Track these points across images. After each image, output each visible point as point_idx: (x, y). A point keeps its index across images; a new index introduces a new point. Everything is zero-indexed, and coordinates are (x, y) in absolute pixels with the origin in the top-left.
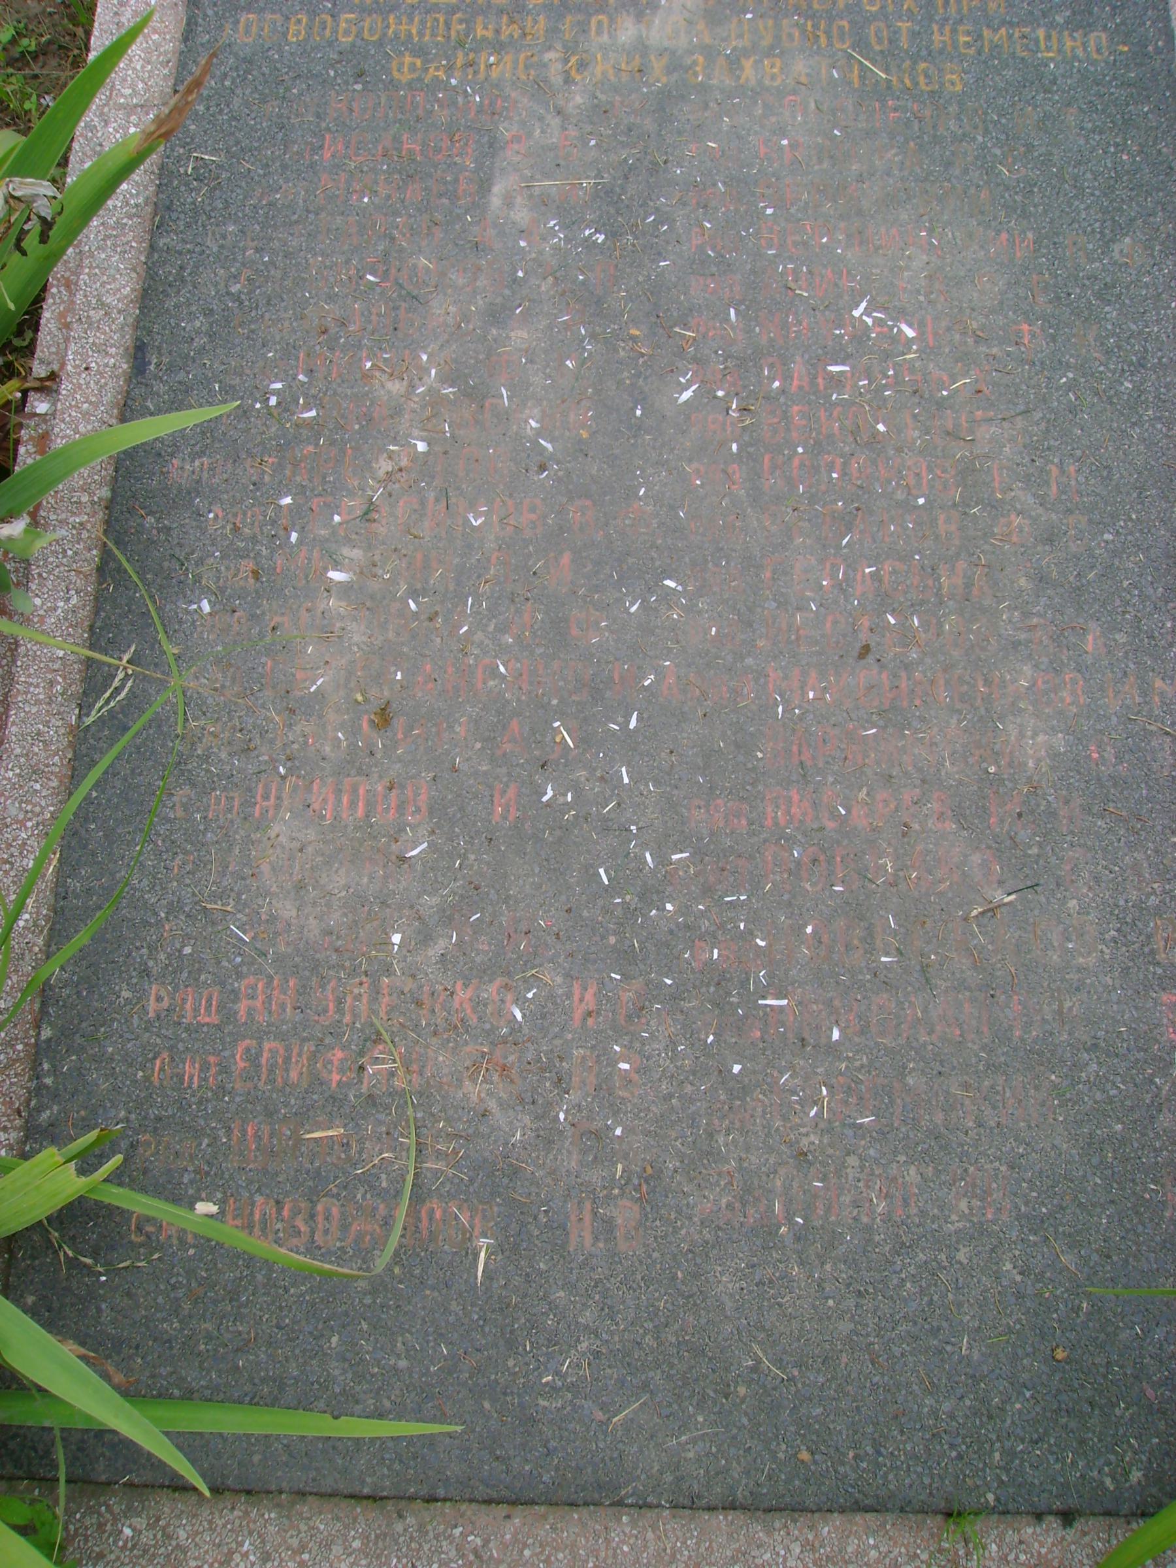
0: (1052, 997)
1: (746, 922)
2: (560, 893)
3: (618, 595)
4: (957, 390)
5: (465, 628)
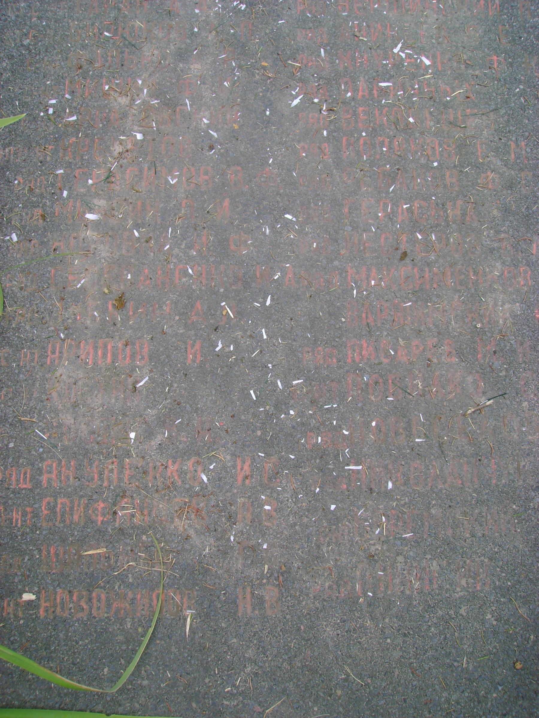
1: (337, 420)
3: (258, 224)
4: (455, 97)
5: (168, 247)
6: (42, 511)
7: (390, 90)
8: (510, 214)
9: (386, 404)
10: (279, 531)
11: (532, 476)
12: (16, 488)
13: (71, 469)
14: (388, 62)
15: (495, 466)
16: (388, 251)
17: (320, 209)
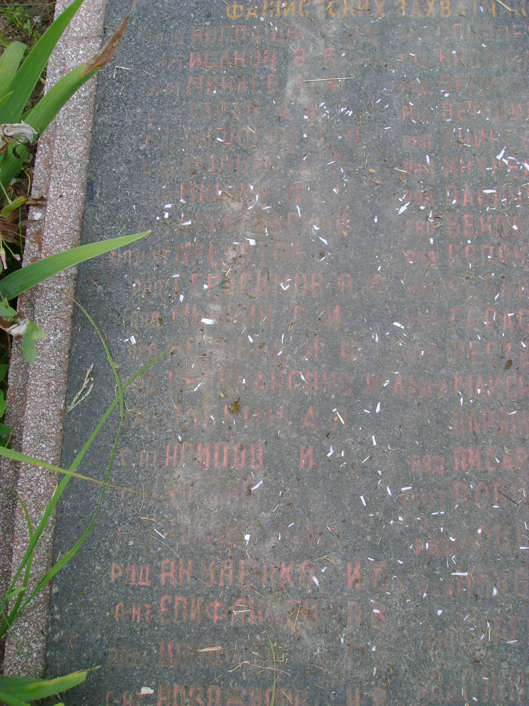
1: (444, 526)
3: (368, 331)
5: (281, 352)
6: (160, 608)
9: (491, 511)
12: (135, 585)
13: (188, 568)
16: (493, 359)
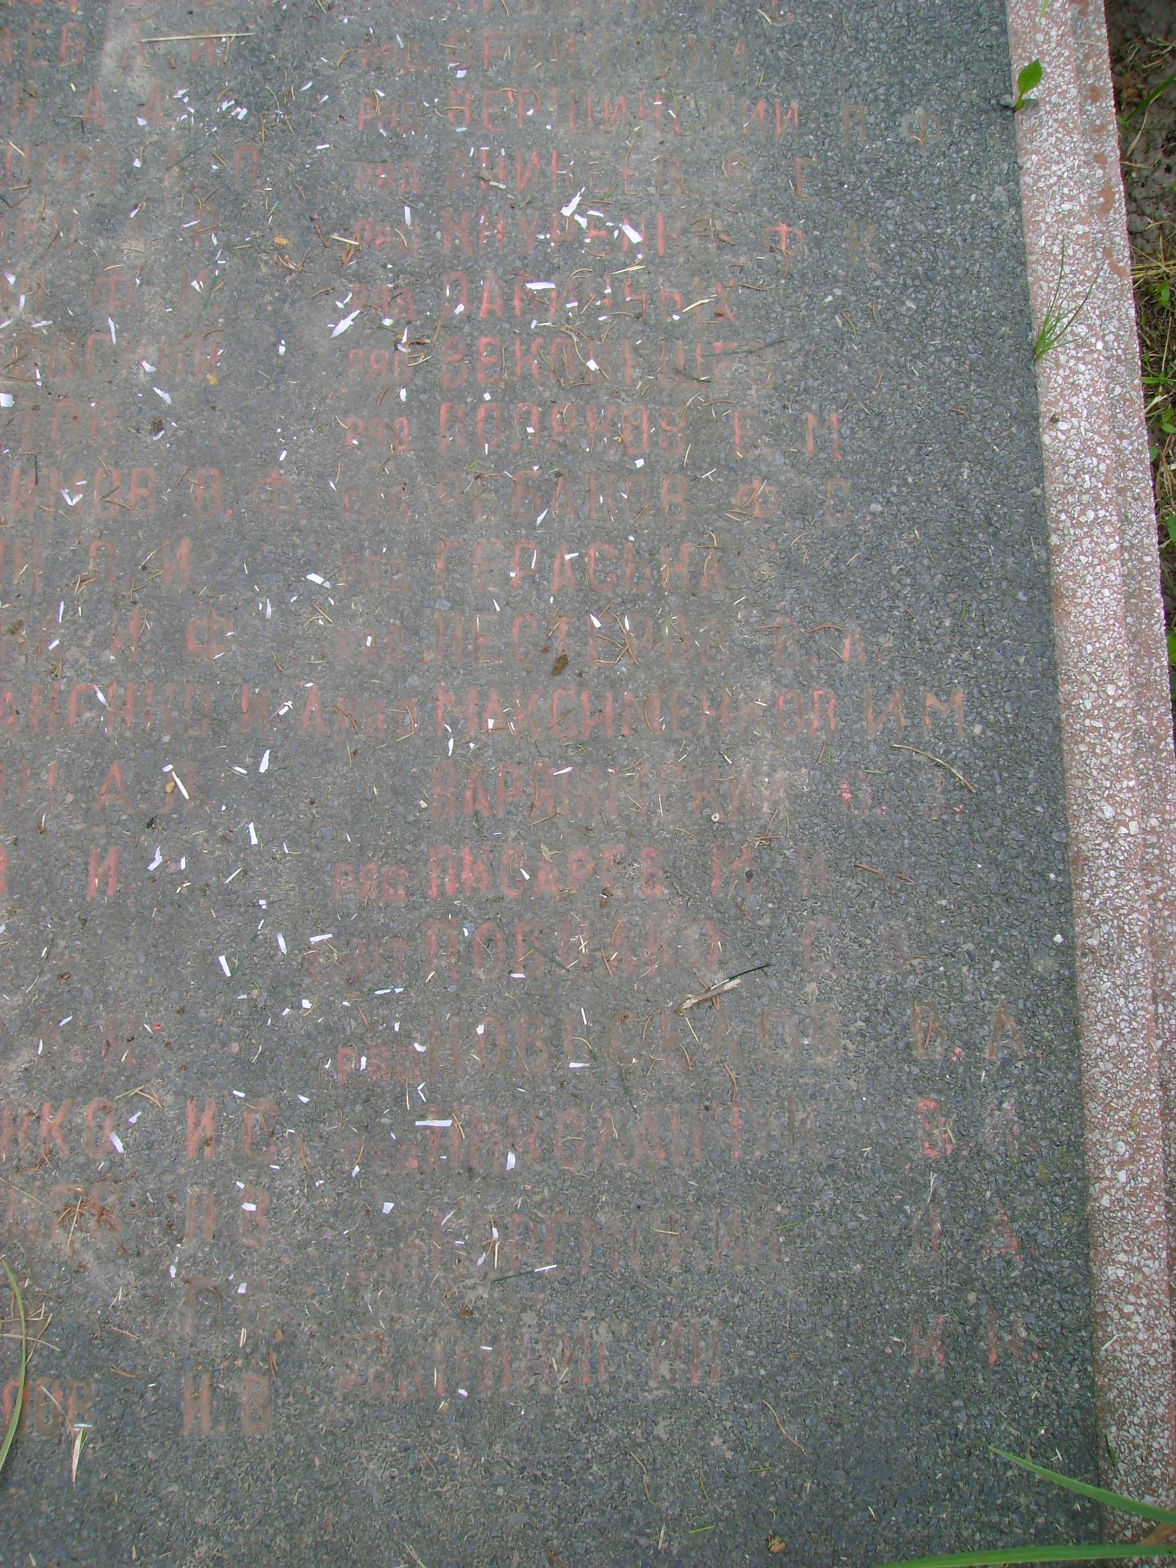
0: (781, 1107)
1: (403, 1021)
2: (171, 988)
3: (250, 594)
5: (56, 643)
7: (549, 299)
8: (798, 574)
10: (272, 1258)
11: (820, 1143)
14: (548, 236)
15: (741, 1122)
16: (527, 653)
17: (384, 561)
